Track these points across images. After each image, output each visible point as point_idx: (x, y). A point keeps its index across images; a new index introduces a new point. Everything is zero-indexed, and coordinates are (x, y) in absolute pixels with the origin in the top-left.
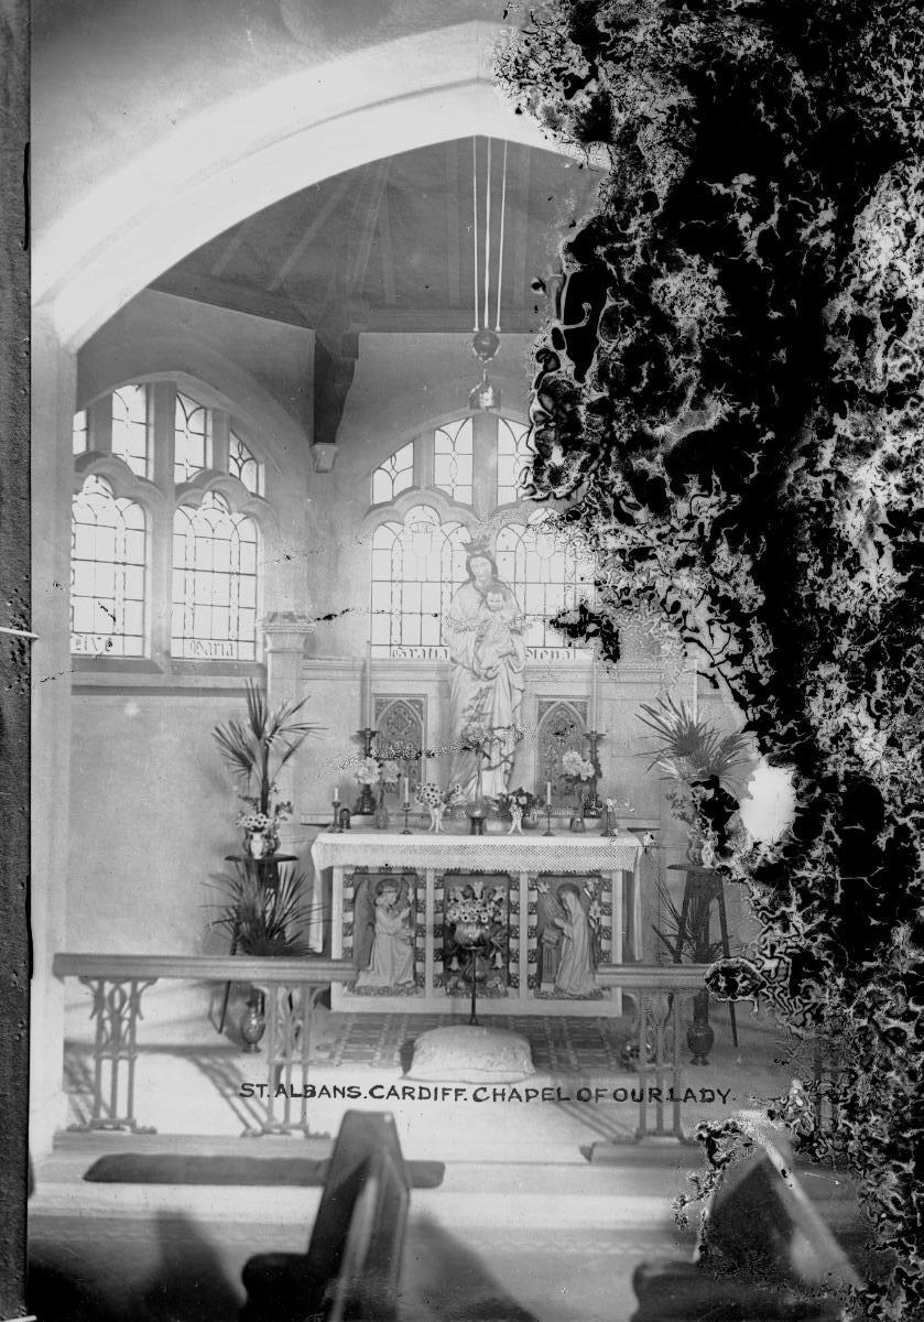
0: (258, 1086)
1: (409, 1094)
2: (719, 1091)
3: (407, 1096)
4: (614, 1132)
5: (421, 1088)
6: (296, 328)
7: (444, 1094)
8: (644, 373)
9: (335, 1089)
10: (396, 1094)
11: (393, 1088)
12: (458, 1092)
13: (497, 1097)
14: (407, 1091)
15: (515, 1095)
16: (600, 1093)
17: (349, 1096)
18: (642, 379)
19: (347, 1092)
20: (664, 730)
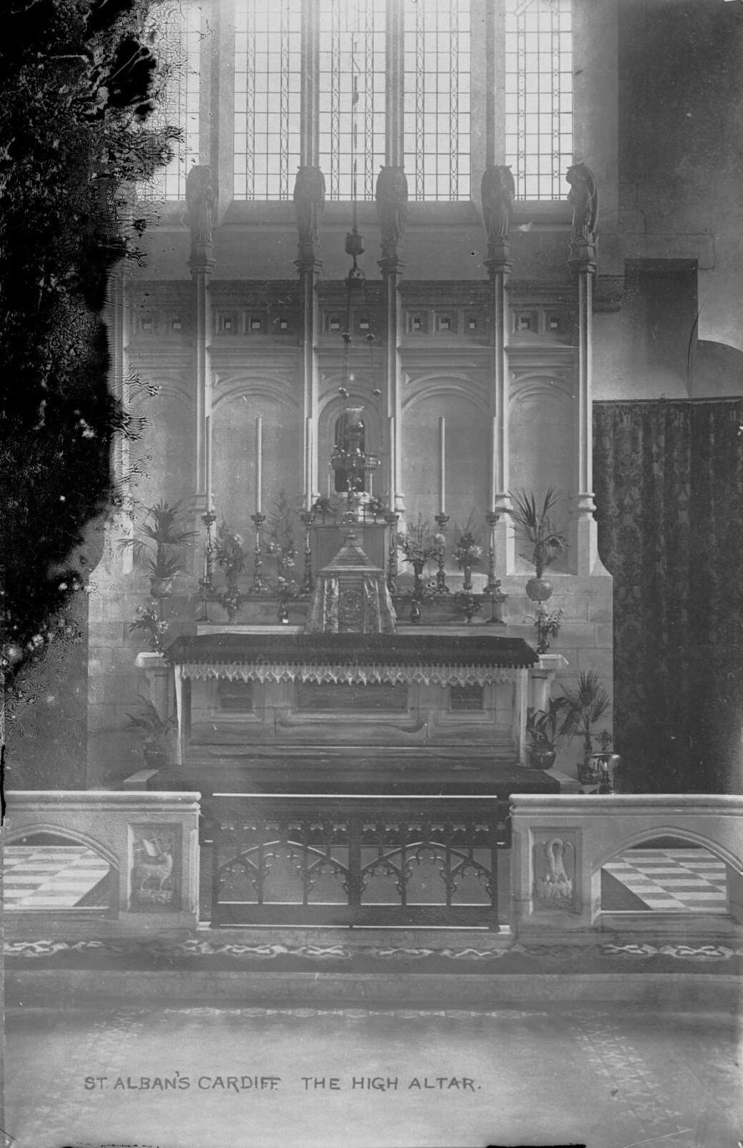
0: (98, 1079)
1: (470, 1085)
2: (124, 1088)
3: (468, 1086)
4: (74, 893)
5: (243, 1078)
6: (606, 976)
7: (262, 1083)
8: (42, 411)
9: (167, 1081)
10: (418, 1085)
11: (119, 1079)
12: (454, 1082)
13: (356, 1085)
14: (144, 1081)
15: (219, 1081)
16: (265, 1081)
17: (180, 1087)
18: (39, 418)
19: (178, 1084)
20: (532, 509)
